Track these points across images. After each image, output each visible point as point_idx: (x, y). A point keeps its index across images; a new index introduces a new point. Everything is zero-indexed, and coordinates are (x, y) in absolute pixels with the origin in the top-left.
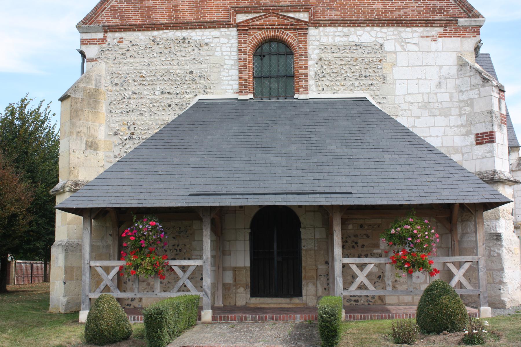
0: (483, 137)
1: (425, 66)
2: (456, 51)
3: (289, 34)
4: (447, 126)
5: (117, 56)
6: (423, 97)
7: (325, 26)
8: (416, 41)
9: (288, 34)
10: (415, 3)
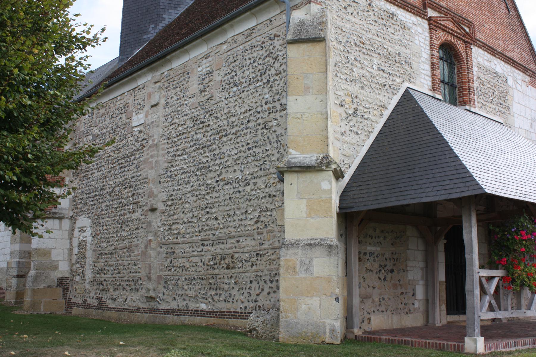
7: (478, 47)
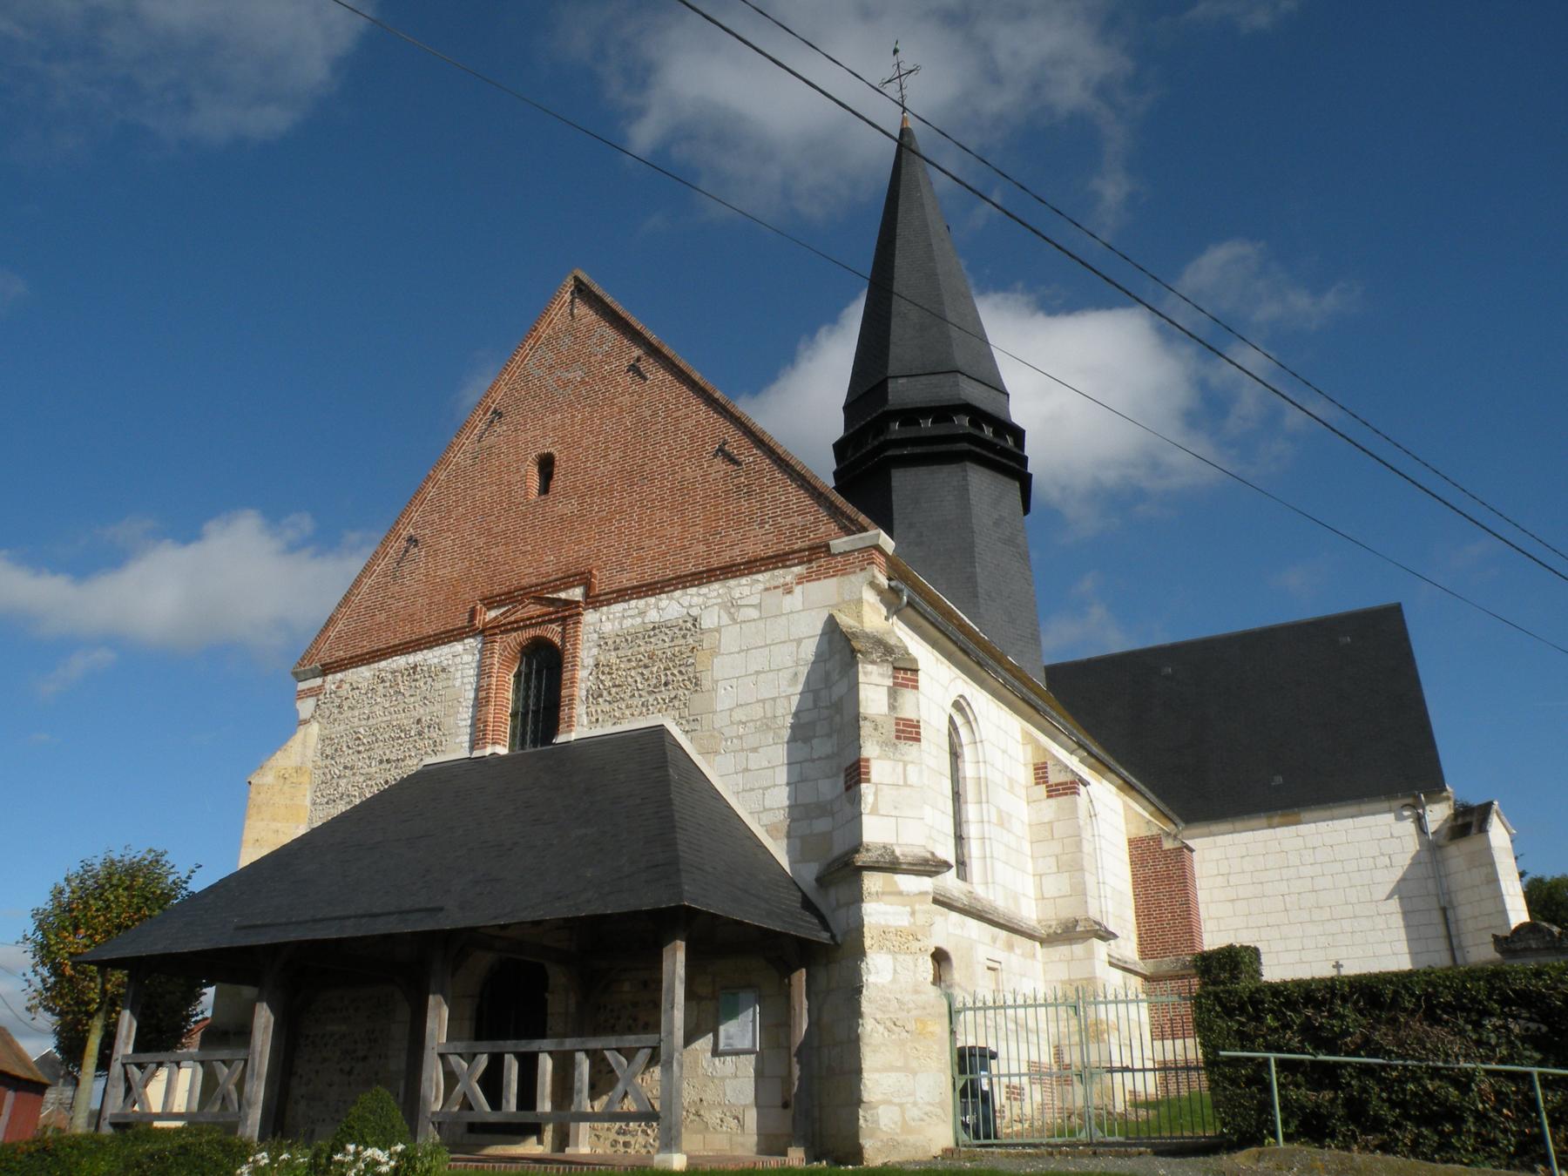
1: (770, 645)
2: (826, 606)
7: (609, 604)
8: (755, 600)
10: (759, 528)
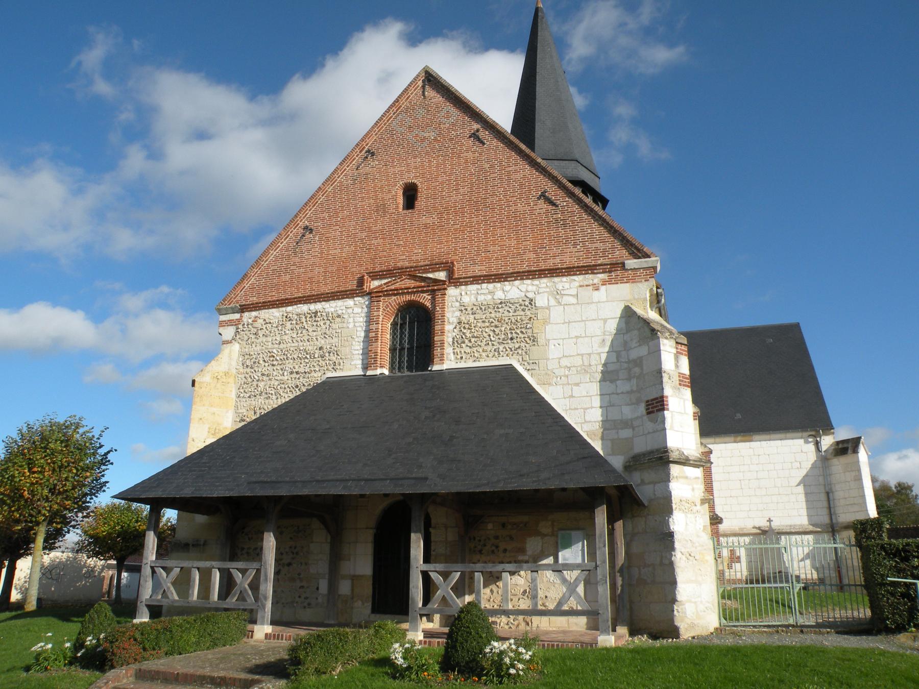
0: (653, 404)
3: (427, 297)
4: (613, 393)
5: (250, 336)
6: (582, 359)
8: (574, 292)
9: (425, 297)
